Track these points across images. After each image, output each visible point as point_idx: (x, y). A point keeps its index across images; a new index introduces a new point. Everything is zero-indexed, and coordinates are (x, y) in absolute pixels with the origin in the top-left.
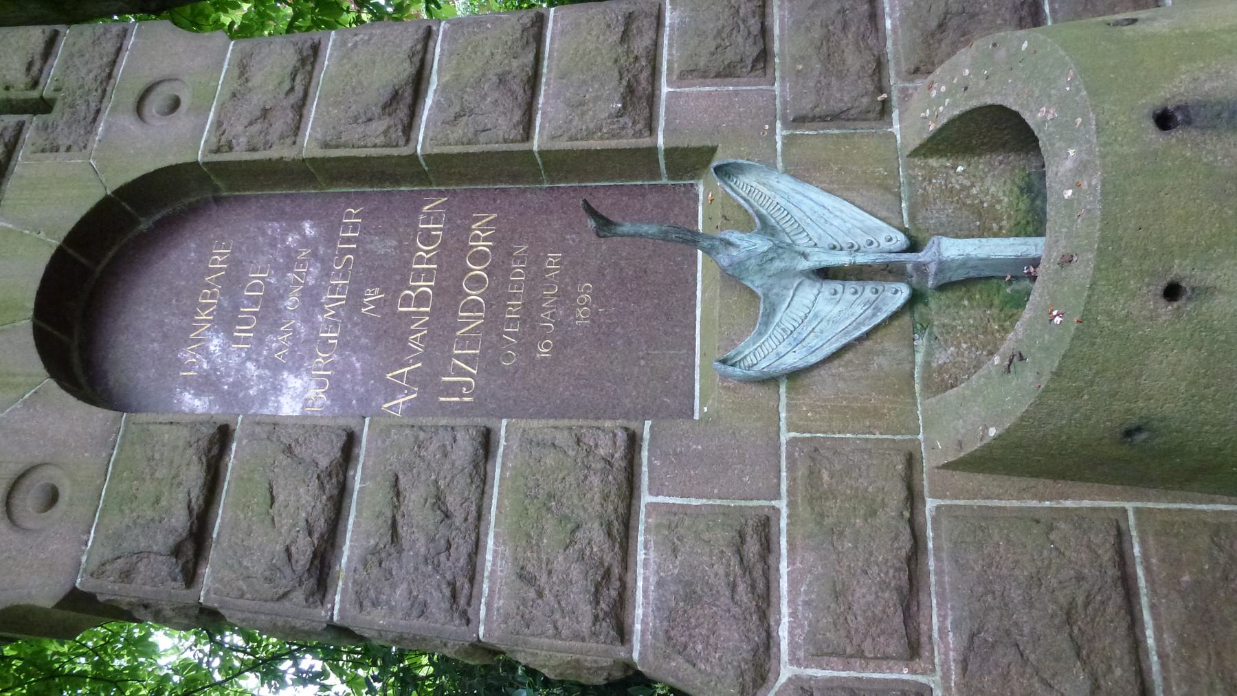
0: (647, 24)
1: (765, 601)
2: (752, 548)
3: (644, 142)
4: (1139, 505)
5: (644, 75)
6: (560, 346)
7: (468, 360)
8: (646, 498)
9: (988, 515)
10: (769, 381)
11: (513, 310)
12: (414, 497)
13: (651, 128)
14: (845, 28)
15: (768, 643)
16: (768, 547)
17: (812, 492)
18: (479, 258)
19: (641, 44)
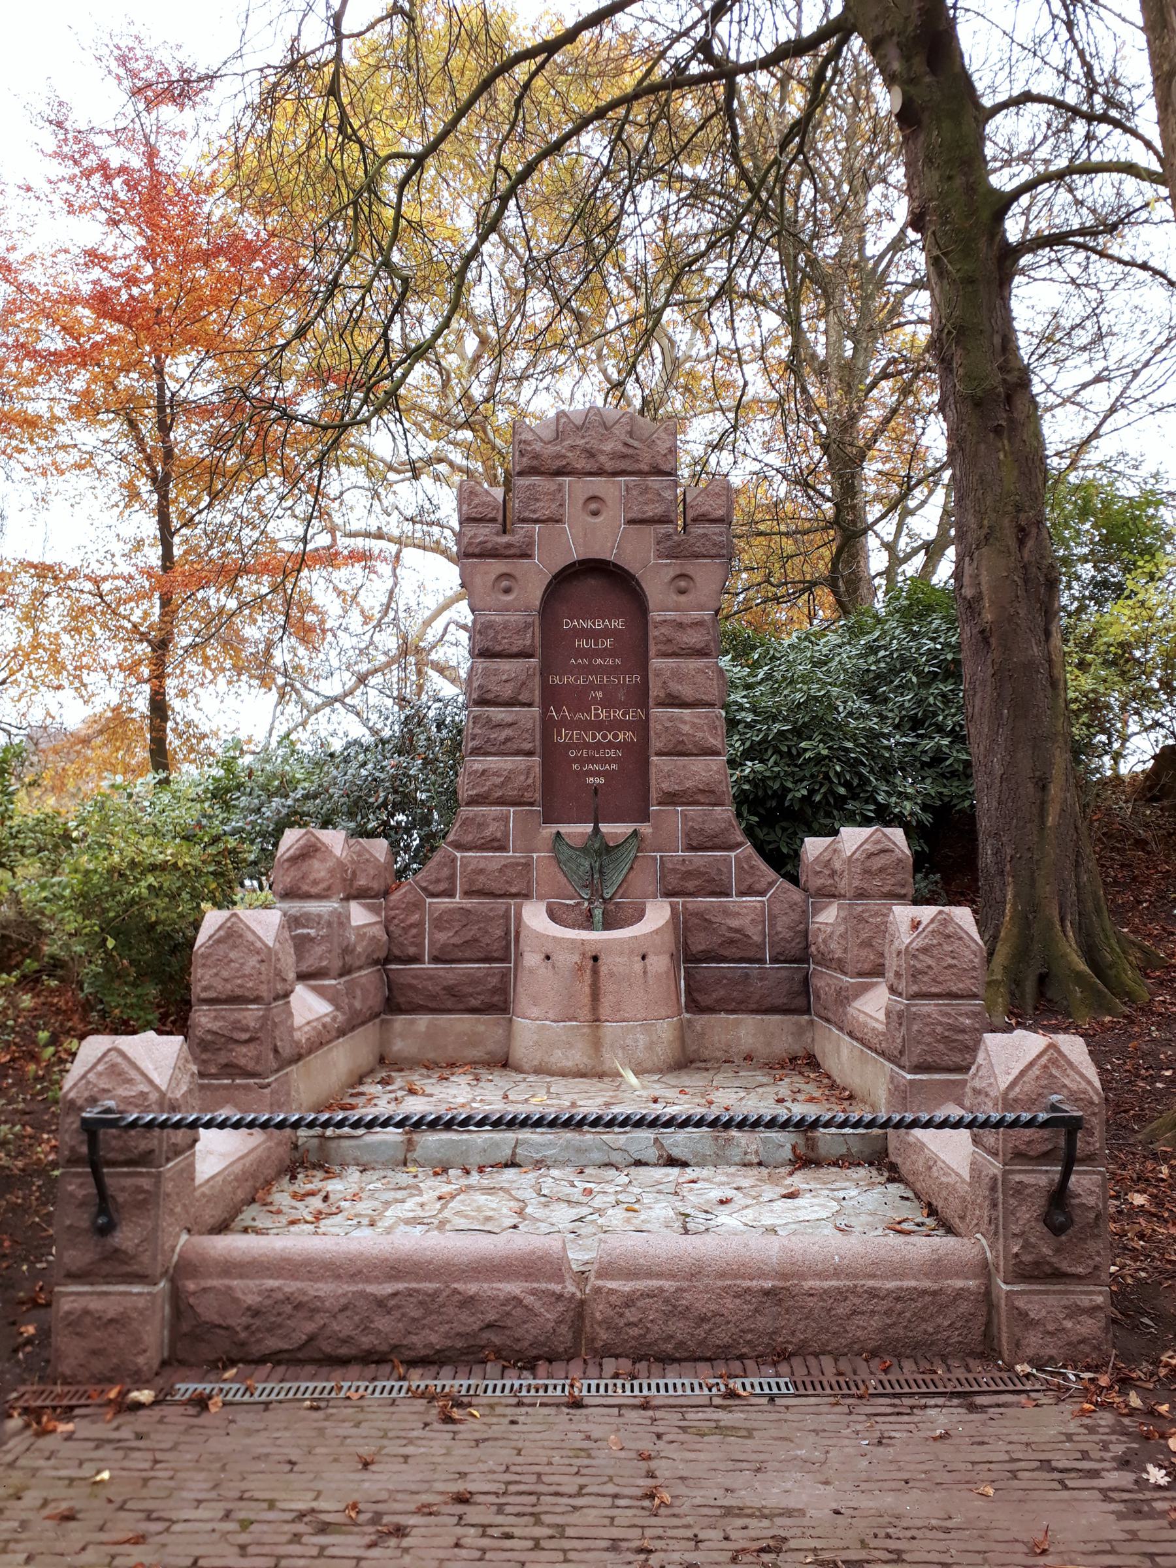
12: (508, 732)
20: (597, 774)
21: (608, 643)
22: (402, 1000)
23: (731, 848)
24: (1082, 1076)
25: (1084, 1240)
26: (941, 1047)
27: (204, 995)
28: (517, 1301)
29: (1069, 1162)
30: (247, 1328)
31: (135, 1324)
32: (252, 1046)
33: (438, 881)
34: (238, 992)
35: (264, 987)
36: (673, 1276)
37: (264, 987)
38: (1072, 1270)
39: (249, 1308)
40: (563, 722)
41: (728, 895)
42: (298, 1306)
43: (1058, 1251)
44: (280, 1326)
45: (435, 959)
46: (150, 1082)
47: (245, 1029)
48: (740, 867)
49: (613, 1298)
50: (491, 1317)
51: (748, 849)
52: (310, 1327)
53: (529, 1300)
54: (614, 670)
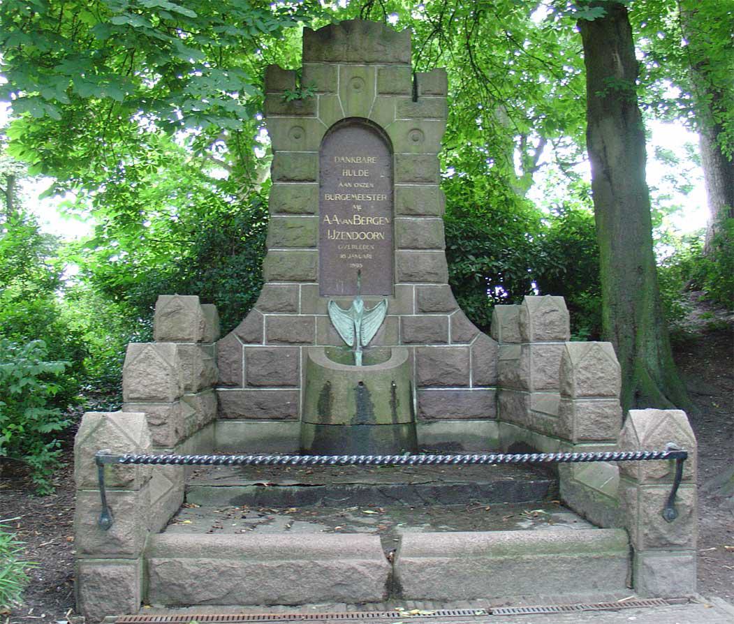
0: (436, 279)
1: (279, 311)
2: (290, 308)
3: (397, 281)
4: (348, 368)
5: (417, 279)
6: (345, 261)
7: (340, 237)
8: (300, 285)
9: (298, 358)
10: (328, 313)
11: (354, 247)
12: (299, 231)
13: (401, 281)
14: (432, 334)
15: (270, 311)
16: (290, 311)
17: (303, 321)
18: (370, 236)
19: (427, 277)
20: (358, 261)
21: (365, 173)
22: (228, 411)
23: (448, 311)
24: (686, 433)
25: (684, 525)
26: (594, 426)
27: (131, 396)
28: (354, 570)
29: (678, 480)
30: (191, 585)
31: (126, 581)
32: (163, 428)
33: (251, 332)
34: (153, 394)
35: (169, 391)
36: (446, 555)
37: (169, 391)
38: (676, 542)
39: (192, 574)
40: (335, 226)
41: (446, 343)
42: (222, 574)
43: (669, 531)
44: (211, 585)
45: (250, 385)
46: (131, 440)
47: (158, 418)
48: (453, 323)
49: (412, 568)
50: (339, 579)
51: (459, 312)
52: (230, 585)
53: (361, 569)
54: (369, 191)
